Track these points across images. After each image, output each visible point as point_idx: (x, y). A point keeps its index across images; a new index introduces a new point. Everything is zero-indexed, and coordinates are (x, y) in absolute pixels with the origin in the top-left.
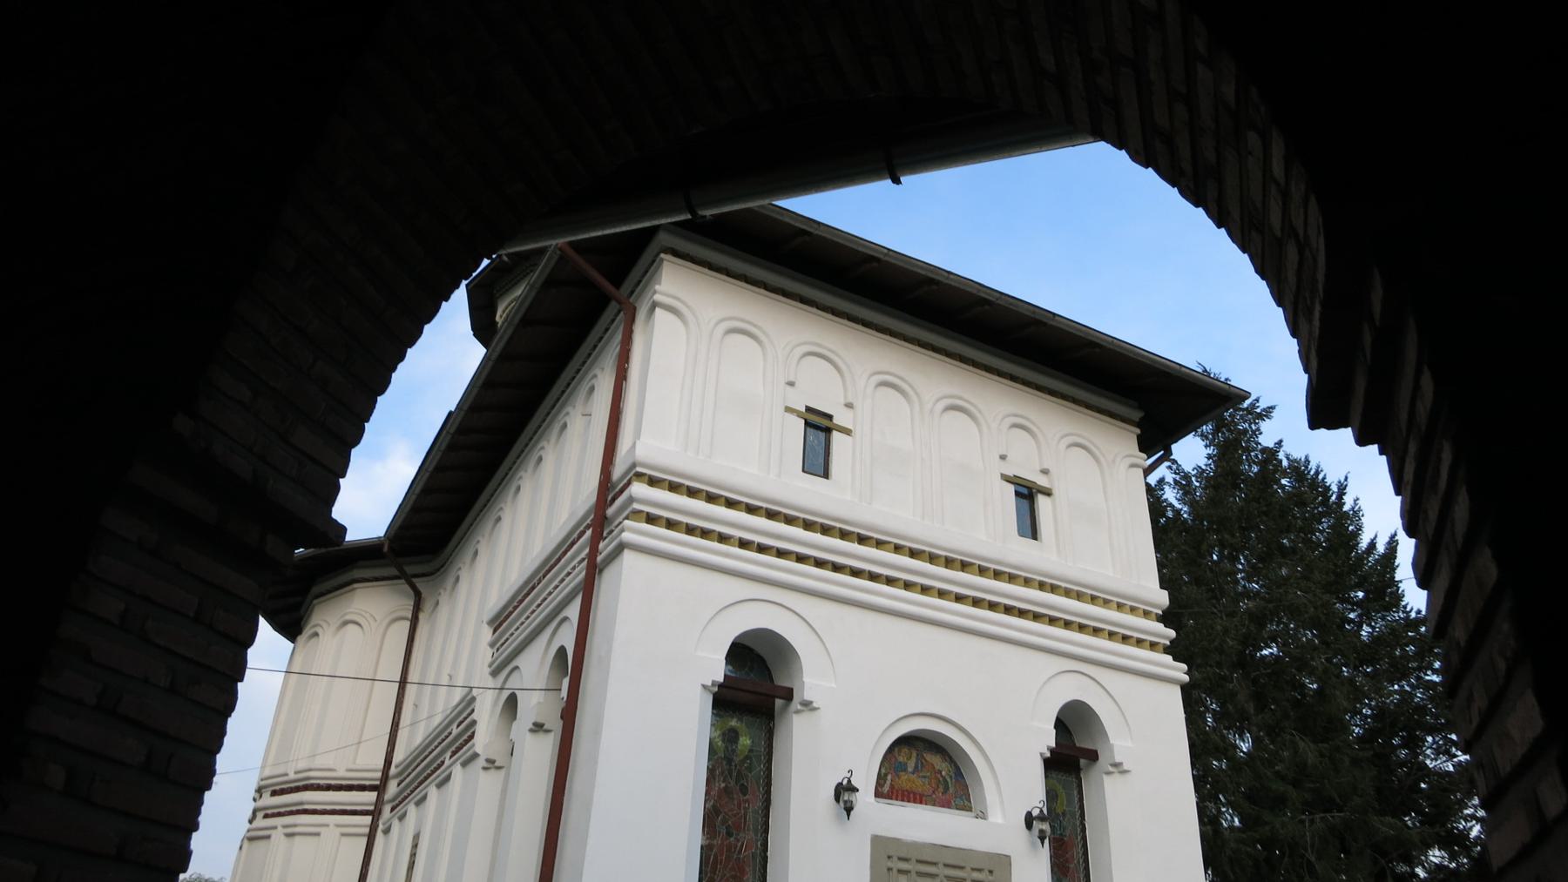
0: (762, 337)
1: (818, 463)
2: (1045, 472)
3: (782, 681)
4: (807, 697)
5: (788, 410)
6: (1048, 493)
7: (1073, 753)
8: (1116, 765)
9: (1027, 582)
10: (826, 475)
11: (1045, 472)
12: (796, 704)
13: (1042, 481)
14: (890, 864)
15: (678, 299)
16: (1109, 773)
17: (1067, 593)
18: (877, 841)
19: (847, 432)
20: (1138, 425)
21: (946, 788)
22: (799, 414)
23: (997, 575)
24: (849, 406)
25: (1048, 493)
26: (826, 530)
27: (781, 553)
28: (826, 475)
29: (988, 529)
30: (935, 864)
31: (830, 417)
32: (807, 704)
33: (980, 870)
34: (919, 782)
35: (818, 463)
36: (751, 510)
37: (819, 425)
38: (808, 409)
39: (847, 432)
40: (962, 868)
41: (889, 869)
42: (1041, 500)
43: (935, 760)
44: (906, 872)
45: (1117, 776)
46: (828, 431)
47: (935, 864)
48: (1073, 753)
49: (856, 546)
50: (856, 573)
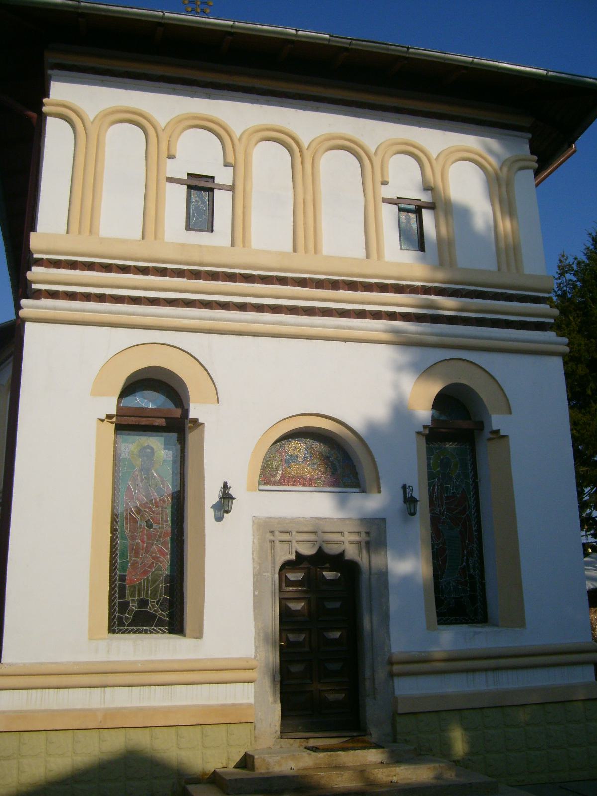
1: (200, 218)
3: (434, 411)
4: (495, 427)
12: (486, 434)
16: (489, 439)
31: (213, 178)
32: (195, 421)
35: (200, 218)
46: (211, 190)
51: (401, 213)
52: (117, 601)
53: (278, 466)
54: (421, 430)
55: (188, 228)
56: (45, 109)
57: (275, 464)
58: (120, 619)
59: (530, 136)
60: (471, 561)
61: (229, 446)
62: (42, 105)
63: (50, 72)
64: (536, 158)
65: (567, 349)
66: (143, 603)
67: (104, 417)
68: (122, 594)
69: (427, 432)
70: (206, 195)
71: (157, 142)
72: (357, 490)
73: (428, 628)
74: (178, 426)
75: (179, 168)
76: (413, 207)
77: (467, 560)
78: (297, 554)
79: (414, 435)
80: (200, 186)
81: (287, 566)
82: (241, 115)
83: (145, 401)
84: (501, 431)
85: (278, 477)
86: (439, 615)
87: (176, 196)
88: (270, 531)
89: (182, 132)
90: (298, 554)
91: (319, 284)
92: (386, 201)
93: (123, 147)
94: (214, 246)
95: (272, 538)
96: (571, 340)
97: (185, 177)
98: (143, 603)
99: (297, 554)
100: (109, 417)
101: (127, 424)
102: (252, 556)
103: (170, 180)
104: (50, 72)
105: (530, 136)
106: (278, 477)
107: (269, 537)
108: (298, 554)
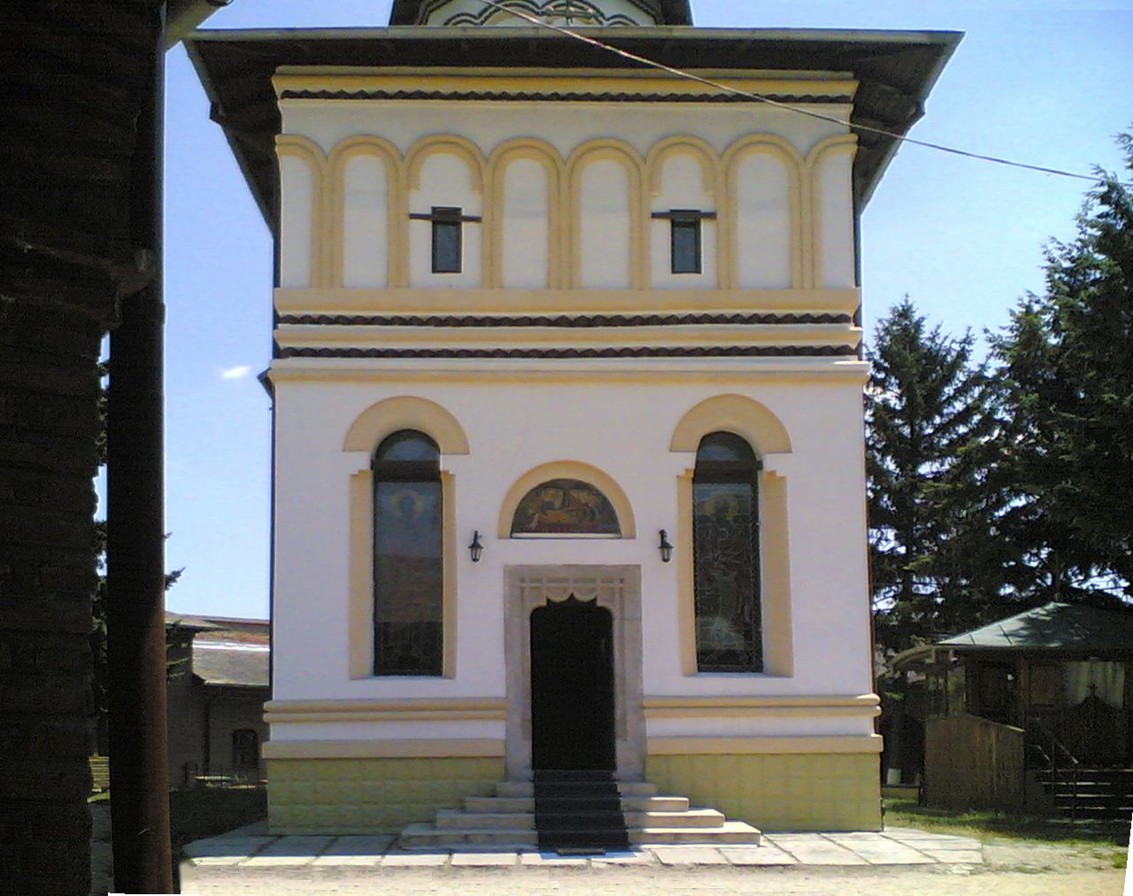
7: (729, 470)
25: (711, 216)
42: (705, 226)
46: (457, 225)
48: (729, 470)
51: (440, 228)
53: (534, 514)
55: (434, 270)
57: (530, 511)
61: (477, 494)
67: (357, 473)
71: (402, 166)
73: (506, 566)
74: (427, 474)
75: (423, 202)
77: (743, 607)
78: (548, 601)
79: (774, 469)
80: (446, 221)
82: (486, 123)
84: (457, 478)
85: (533, 525)
87: (422, 232)
88: (519, 578)
93: (364, 173)
94: (460, 291)
96: (1033, 304)
99: (548, 601)
101: (702, 474)
102: (675, 752)
103: (413, 216)
106: (533, 525)
107: (519, 584)
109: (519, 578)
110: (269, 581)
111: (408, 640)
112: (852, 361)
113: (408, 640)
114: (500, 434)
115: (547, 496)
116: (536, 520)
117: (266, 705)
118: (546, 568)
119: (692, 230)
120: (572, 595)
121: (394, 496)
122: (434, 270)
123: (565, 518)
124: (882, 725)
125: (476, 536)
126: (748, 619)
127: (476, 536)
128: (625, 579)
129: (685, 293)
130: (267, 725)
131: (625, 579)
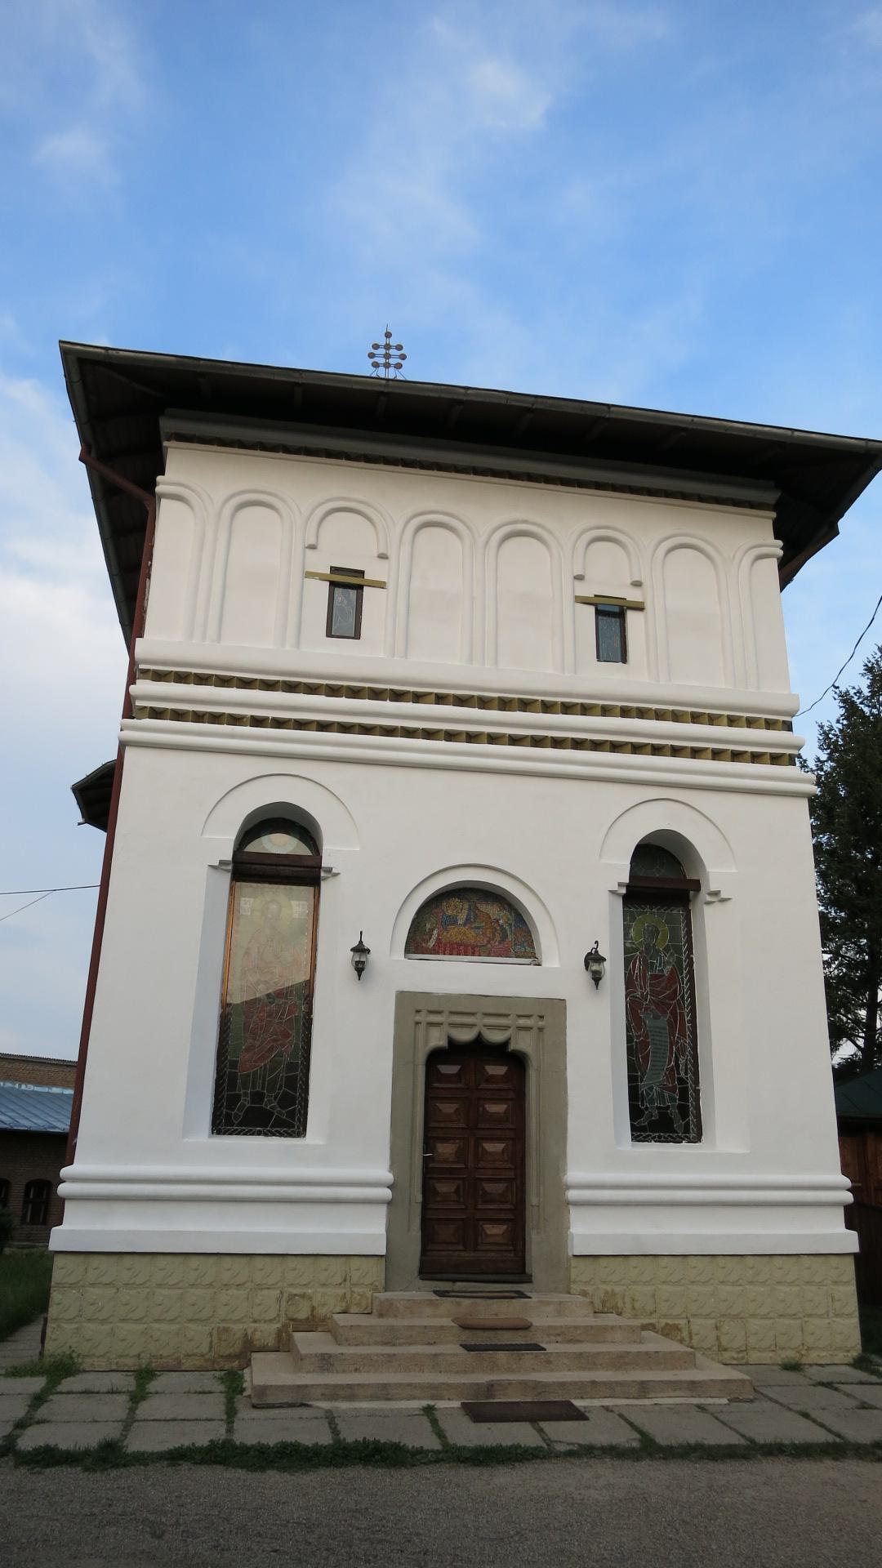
0: (708, 548)
1: (613, 644)
2: (637, 584)
3: (691, 876)
4: (713, 888)
5: (309, 575)
6: (639, 607)
7: (663, 882)
8: (716, 894)
9: (606, 711)
10: (624, 661)
11: (637, 584)
12: (704, 895)
13: (633, 595)
14: (418, 1018)
15: (539, 525)
16: (709, 903)
17: (659, 715)
18: (403, 998)
19: (381, 585)
20: (775, 508)
21: (504, 937)
22: (322, 577)
23: (567, 709)
24: (383, 556)
25: (639, 607)
26: (355, 693)
27: (301, 725)
28: (624, 661)
29: (561, 660)
30: (473, 1014)
31: (362, 573)
32: (329, 870)
33: (528, 1016)
34: (472, 933)
35: (613, 644)
36: (440, 699)
37: (347, 583)
38: (334, 570)
39: (381, 585)
40: (507, 1016)
41: (417, 1023)
42: (631, 616)
43: (492, 910)
44: (528, 1029)
45: (717, 906)
46: (360, 588)
47: (473, 1014)
48: (663, 882)
49: (410, 705)
50: (389, 732)
51: (338, 591)
52: (225, 1094)
54: (616, 888)
55: (329, 634)
56: (158, 489)
57: (428, 926)
58: (228, 1115)
59: (774, 515)
60: (682, 1061)
62: (154, 484)
63: (165, 444)
64: (780, 543)
65: (817, 791)
66: (258, 1097)
68: (232, 1086)
69: (624, 891)
70: (353, 593)
72: (528, 961)
74: (306, 873)
76: (617, 610)
79: (606, 896)
80: (347, 583)
81: (435, 1057)
83: (279, 844)
85: (431, 944)
86: (633, 1128)
88: (413, 1008)
89: (233, 516)
90: (451, 1041)
91: (484, 703)
92: (585, 601)
95: (424, 1025)
97: (328, 571)
98: (258, 1097)
100: (222, 863)
101: (247, 868)
104: (165, 444)
105: (774, 515)
106: (431, 944)
108: (451, 1041)
109: (413, 1008)
110: (602, 785)
111: (259, 1083)
112: (794, 771)
113: (259, 1083)
114: (389, 836)
115: (450, 908)
116: (434, 937)
117: (65, 1172)
118: (448, 997)
119: (615, 621)
120: (480, 1034)
121: (260, 900)
122: (329, 634)
123: (471, 936)
124: (853, 1217)
125: (597, 984)
126: (682, 1074)
127: (597, 984)
128: (548, 1014)
129: (608, 681)
130: (62, 1201)
131: (548, 1014)
